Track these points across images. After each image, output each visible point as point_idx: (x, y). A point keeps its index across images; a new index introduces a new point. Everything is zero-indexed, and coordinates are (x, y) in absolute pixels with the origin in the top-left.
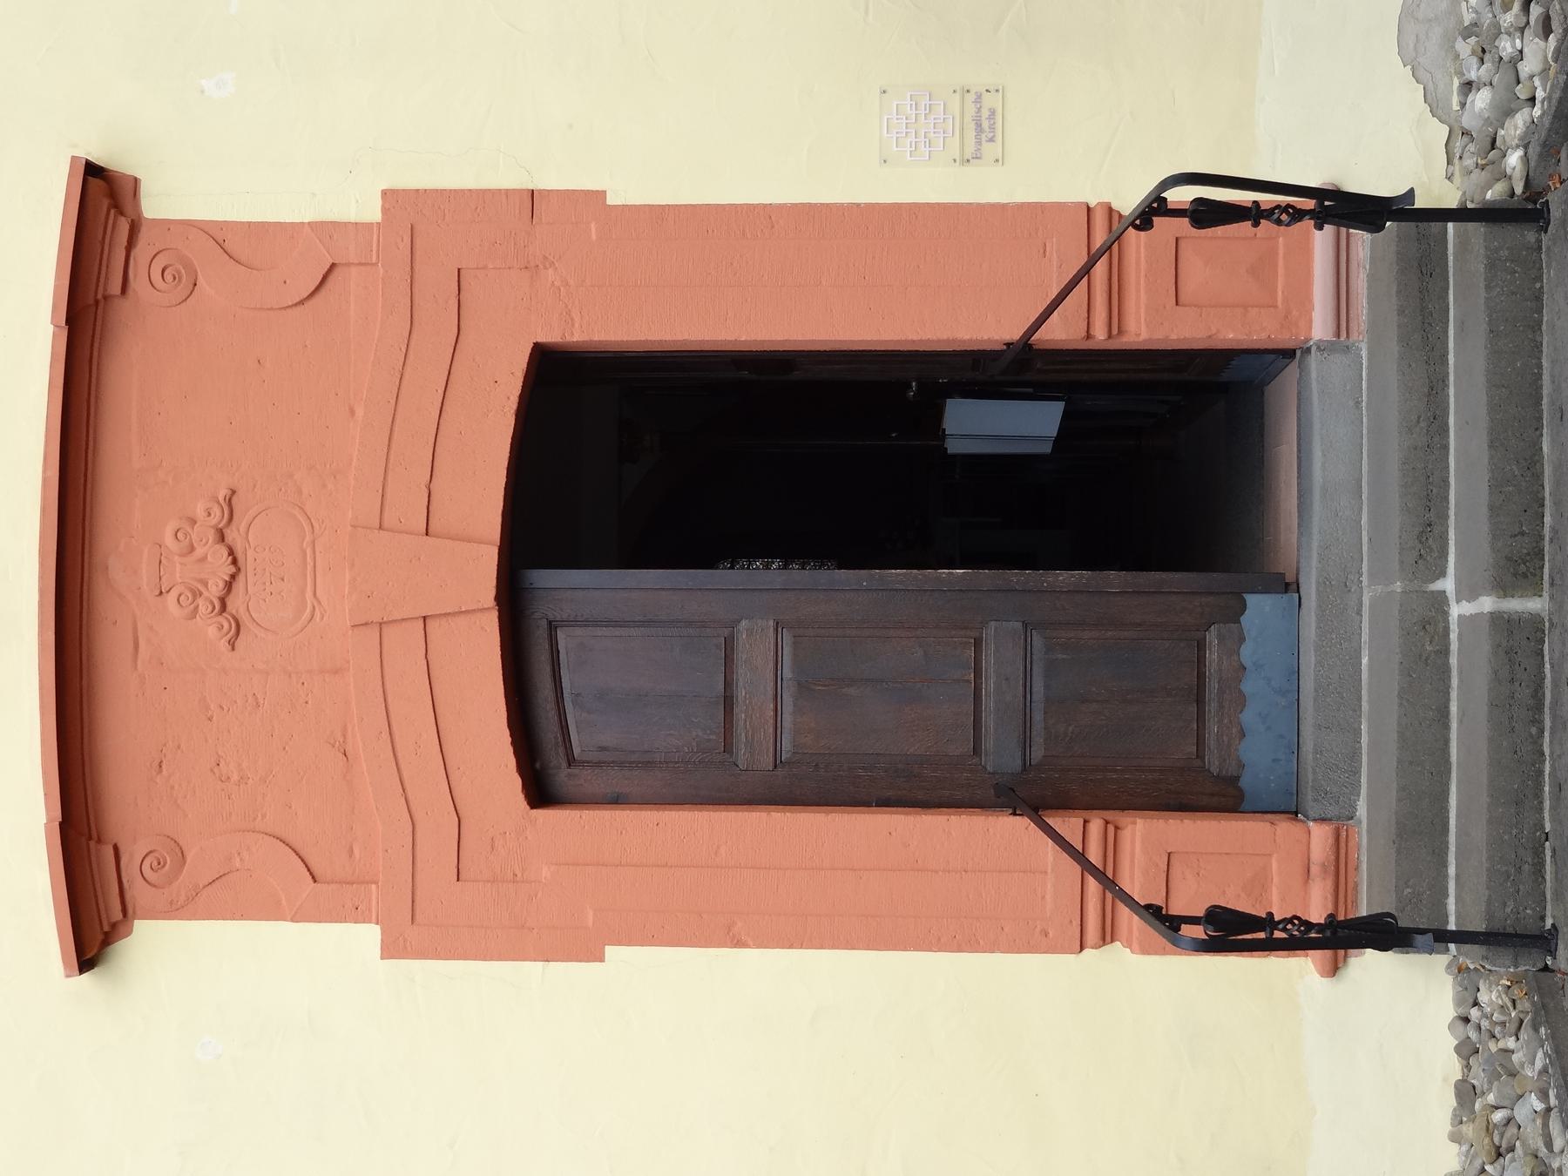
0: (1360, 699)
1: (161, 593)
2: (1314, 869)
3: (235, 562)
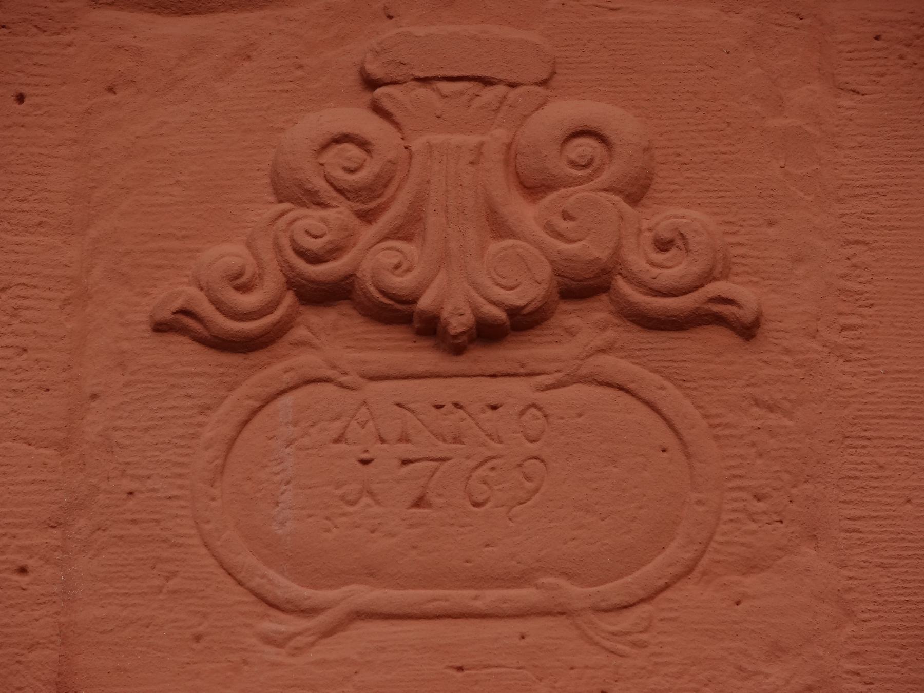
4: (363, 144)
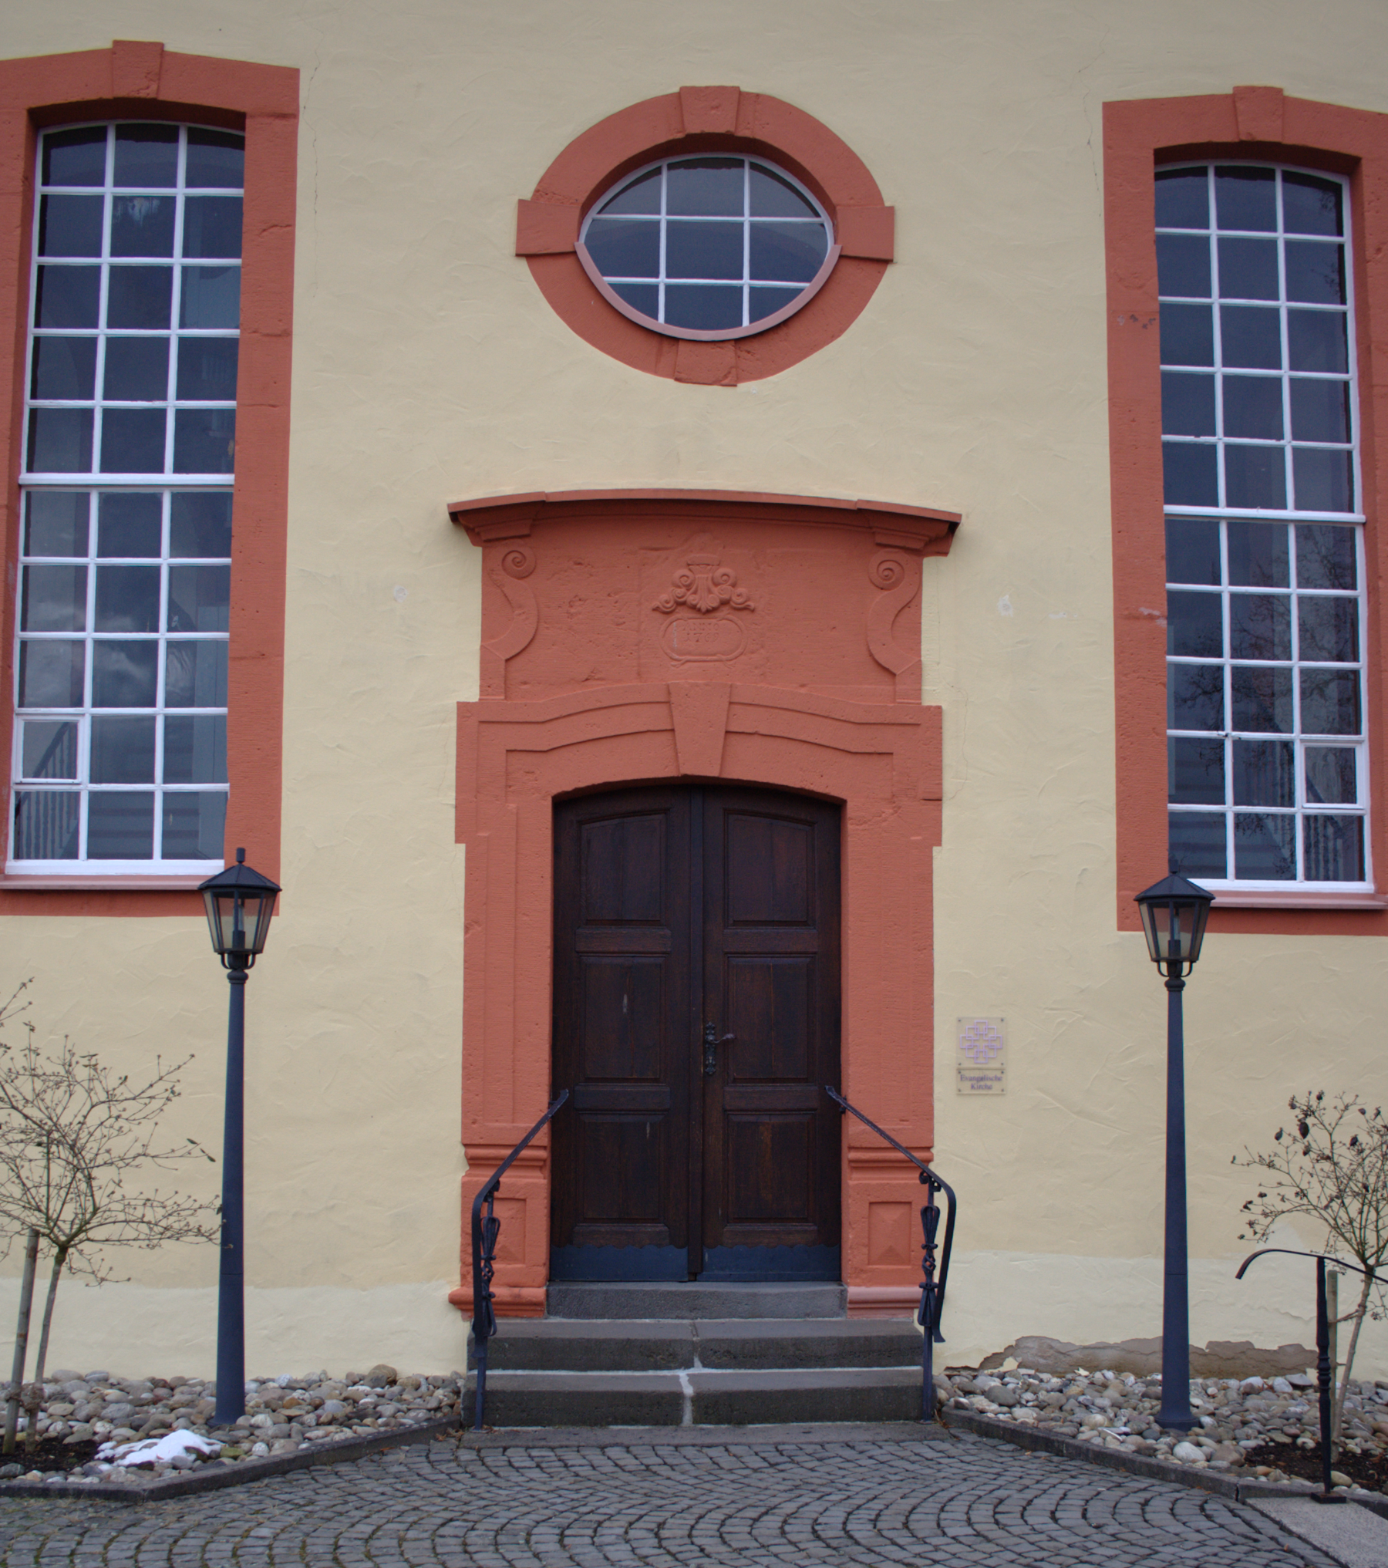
0: (623, 1318)
1: (689, 565)
2: (516, 1290)
3: (708, 611)
4: (688, 577)
